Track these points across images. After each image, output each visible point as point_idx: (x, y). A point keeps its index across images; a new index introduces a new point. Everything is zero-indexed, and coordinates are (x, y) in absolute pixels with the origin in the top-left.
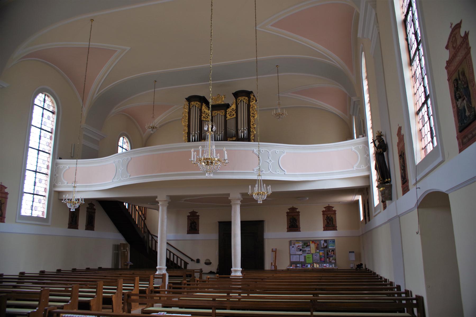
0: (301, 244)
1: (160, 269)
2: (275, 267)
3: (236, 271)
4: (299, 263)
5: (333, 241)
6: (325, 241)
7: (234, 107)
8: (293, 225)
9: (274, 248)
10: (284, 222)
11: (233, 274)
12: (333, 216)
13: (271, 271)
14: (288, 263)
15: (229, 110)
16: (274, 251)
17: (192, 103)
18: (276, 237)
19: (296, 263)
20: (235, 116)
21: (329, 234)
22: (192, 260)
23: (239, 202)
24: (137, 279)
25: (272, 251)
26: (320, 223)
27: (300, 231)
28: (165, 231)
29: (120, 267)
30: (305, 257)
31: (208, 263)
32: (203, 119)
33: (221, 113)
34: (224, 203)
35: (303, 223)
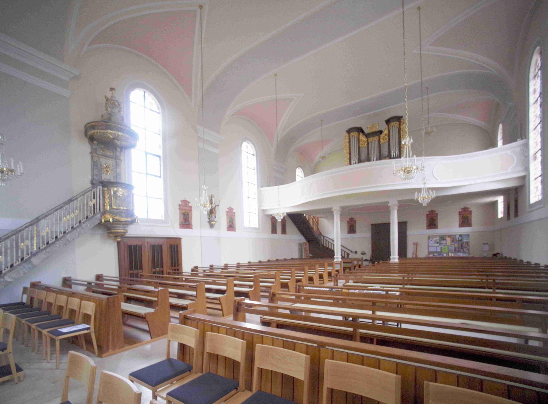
0: (438, 238)
1: (337, 258)
2: (416, 255)
3: (394, 258)
4: (436, 252)
5: (468, 235)
6: (460, 236)
7: (386, 132)
8: (432, 223)
9: (416, 241)
10: (424, 221)
11: (392, 261)
12: (469, 215)
13: (413, 258)
14: (427, 253)
15: (382, 136)
16: (416, 244)
17: (352, 134)
18: (418, 233)
19: (433, 253)
20: (387, 139)
21: (465, 230)
22: (352, 252)
23: (396, 207)
24: (326, 264)
25: (414, 244)
26: (456, 220)
27: (192, 228)
28: (334, 232)
29: (304, 257)
30: (441, 248)
31: (363, 254)
32: (361, 146)
33: (376, 139)
34: (385, 209)
35: (440, 222)
